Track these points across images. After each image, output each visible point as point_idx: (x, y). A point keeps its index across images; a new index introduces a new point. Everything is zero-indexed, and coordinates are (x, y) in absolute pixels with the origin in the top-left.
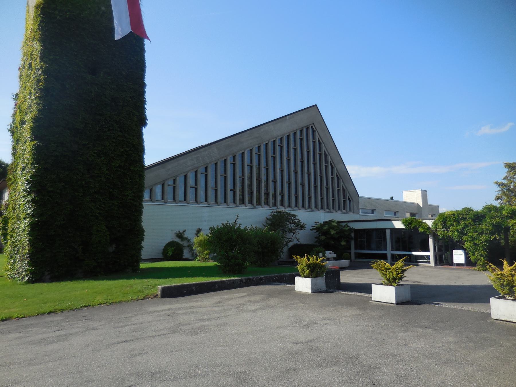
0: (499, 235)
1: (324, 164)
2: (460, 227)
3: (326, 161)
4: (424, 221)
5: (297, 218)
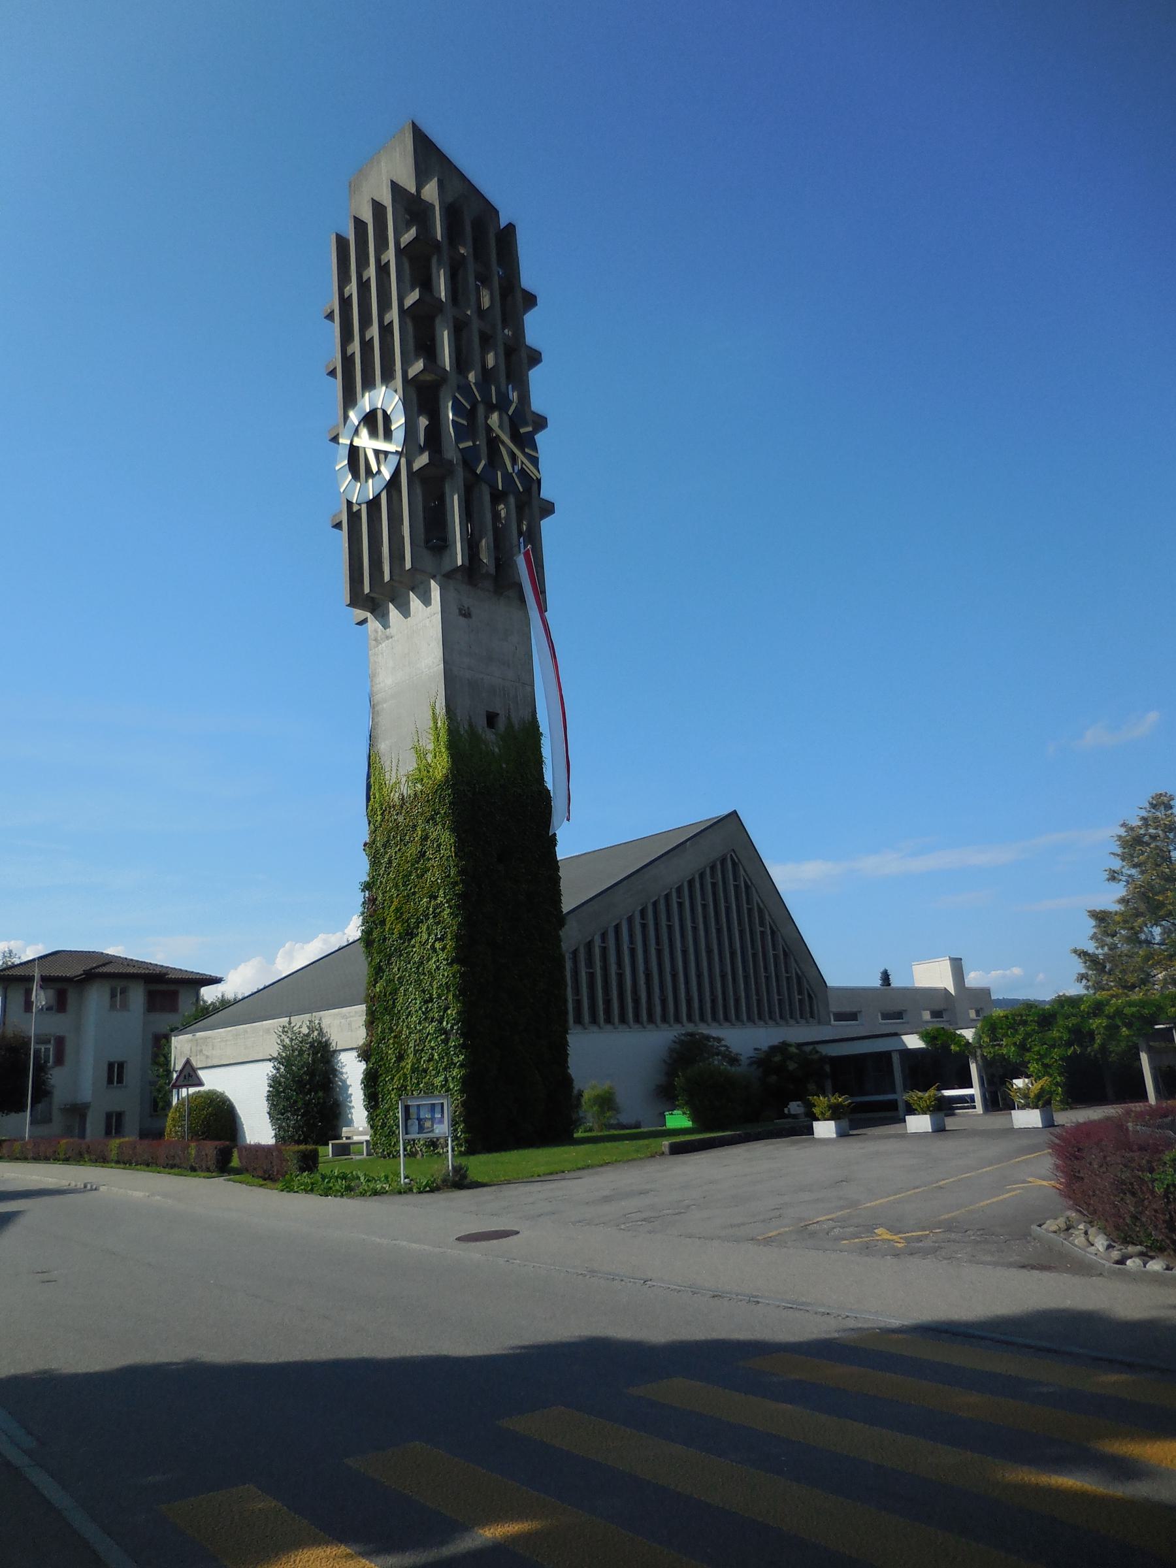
0: (1080, 1045)
1: (759, 929)
2: (1018, 1038)
3: (762, 924)
4: (958, 1032)
5: (723, 1043)
